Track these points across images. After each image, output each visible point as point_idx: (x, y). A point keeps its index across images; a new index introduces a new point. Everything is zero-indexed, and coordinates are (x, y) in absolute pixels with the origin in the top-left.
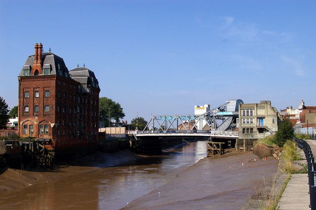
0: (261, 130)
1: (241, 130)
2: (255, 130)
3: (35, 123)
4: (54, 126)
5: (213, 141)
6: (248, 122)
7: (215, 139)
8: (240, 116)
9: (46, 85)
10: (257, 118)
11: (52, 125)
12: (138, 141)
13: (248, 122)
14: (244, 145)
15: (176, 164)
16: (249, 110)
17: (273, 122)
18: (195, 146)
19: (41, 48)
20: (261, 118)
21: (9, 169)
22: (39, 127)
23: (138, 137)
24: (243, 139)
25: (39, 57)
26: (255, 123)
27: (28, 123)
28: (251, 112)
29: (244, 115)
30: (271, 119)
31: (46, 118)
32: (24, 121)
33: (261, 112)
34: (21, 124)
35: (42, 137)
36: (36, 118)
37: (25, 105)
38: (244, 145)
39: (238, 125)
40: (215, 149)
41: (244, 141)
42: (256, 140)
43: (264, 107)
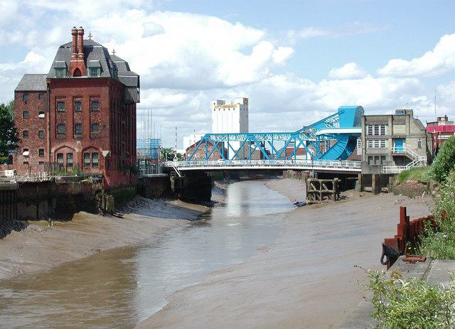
0: (401, 159)
1: (365, 159)
2: (389, 159)
3: (77, 150)
4: (108, 154)
5: (319, 178)
7: (321, 174)
8: (363, 136)
9: (93, 93)
11: (105, 153)
12: (182, 179)
14: (373, 183)
15: (397, 76)
17: (419, 146)
18: (57, 68)
19: (82, 34)
20: (399, 140)
21: (83, 213)
22: (84, 155)
23: (182, 172)
24: (371, 175)
25: (80, 50)
27: (65, 151)
29: (370, 134)
30: (415, 141)
31: (95, 143)
32: (58, 146)
33: (399, 130)
34: (53, 150)
35: (87, 172)
36: (78, 142)
37: (59, 122)
38: (373, 183)
39: (359, 151)
40: (325, 191)
41: (373, 177)
42: (392, 175)
43: (405, 121)
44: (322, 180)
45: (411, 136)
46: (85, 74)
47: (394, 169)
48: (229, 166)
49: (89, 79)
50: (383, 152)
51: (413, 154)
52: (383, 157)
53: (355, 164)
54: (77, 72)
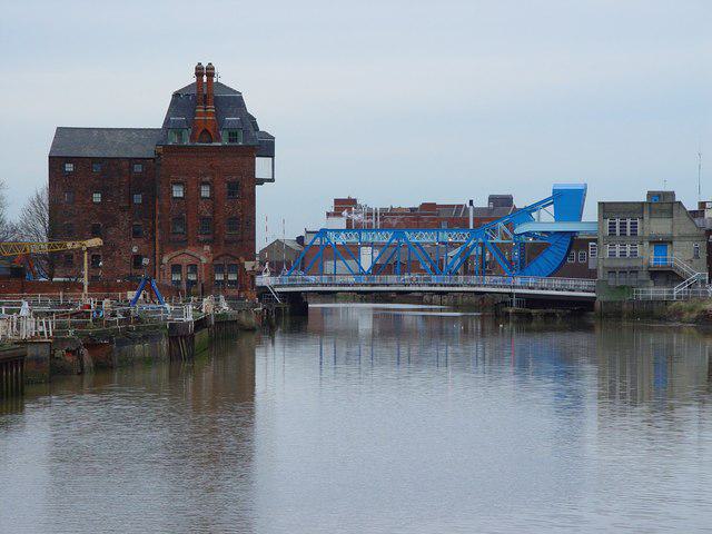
0: (668, 276)
2: (644, 276)
3: (204, 260)
6: (623, 254)
10: (650, 242)
13: (623, 254)
16: (629, 221)
17: (697, 257)
20: (661, 243)
26: (648, 256)
27: (186, 260)
28: (634, 225)
33: (660, 227)
44: (535, 311)
45: (683, 237)
46: (219, 139)
47: (654, 292)
48: (366, 285)
49: (224, 147)
50: (634, 263)
51: (685, 268)
52: (634, 271)
53: (584, 283)
54: (207, 134)
